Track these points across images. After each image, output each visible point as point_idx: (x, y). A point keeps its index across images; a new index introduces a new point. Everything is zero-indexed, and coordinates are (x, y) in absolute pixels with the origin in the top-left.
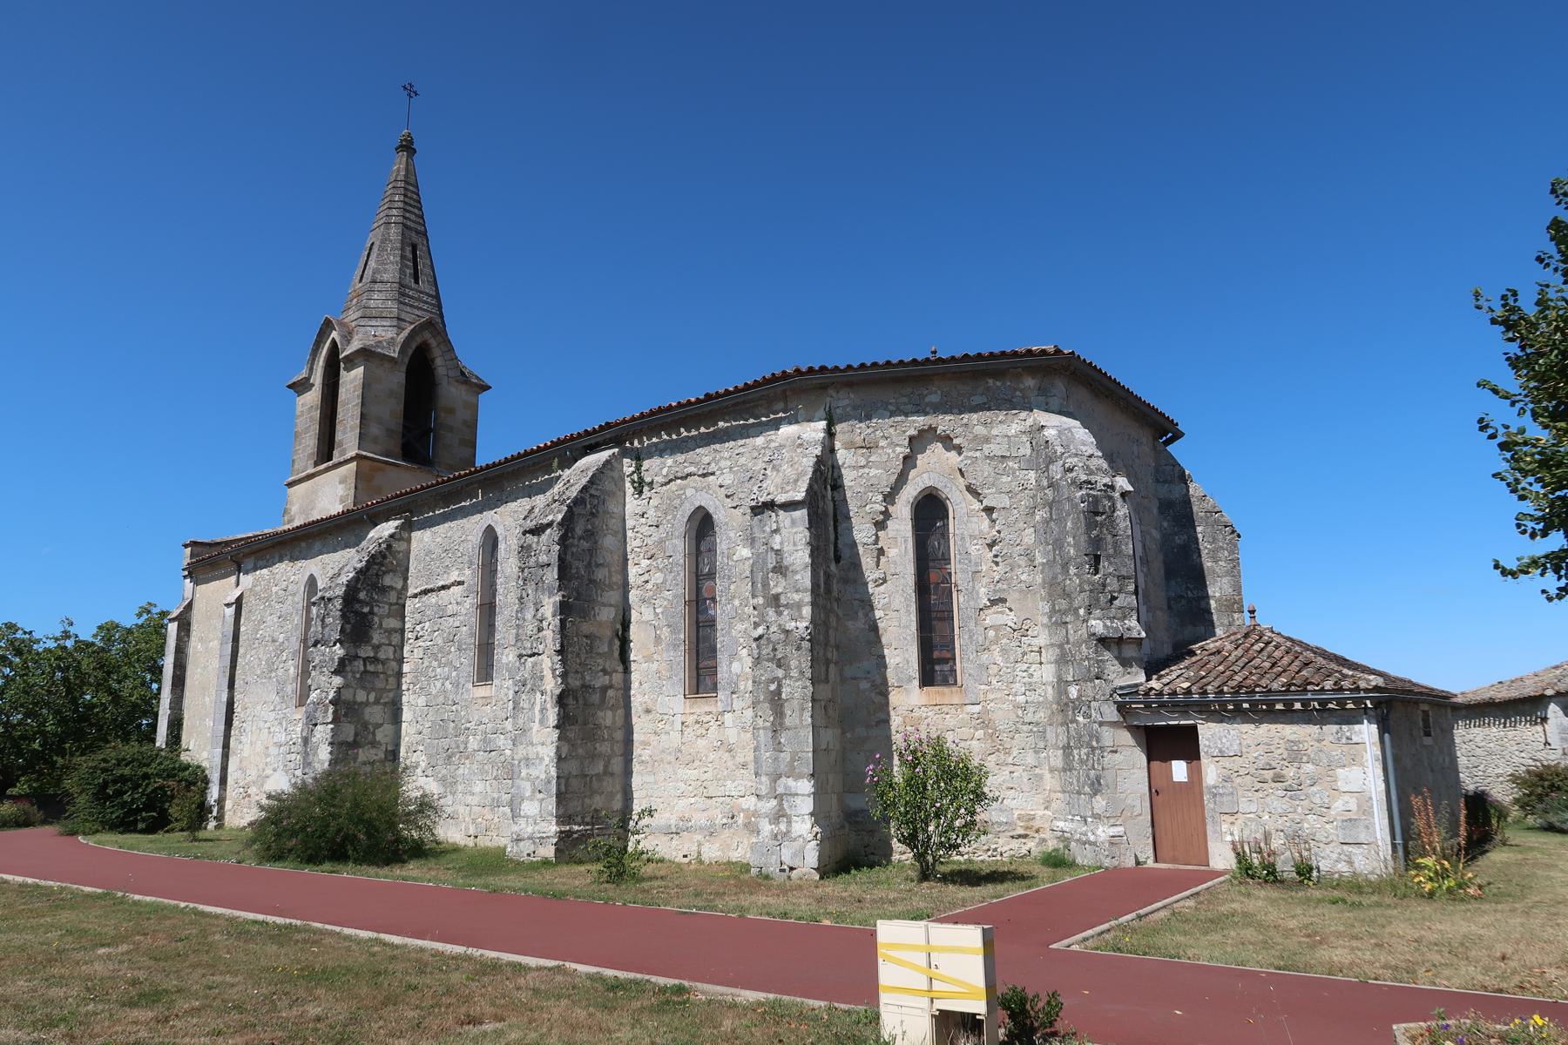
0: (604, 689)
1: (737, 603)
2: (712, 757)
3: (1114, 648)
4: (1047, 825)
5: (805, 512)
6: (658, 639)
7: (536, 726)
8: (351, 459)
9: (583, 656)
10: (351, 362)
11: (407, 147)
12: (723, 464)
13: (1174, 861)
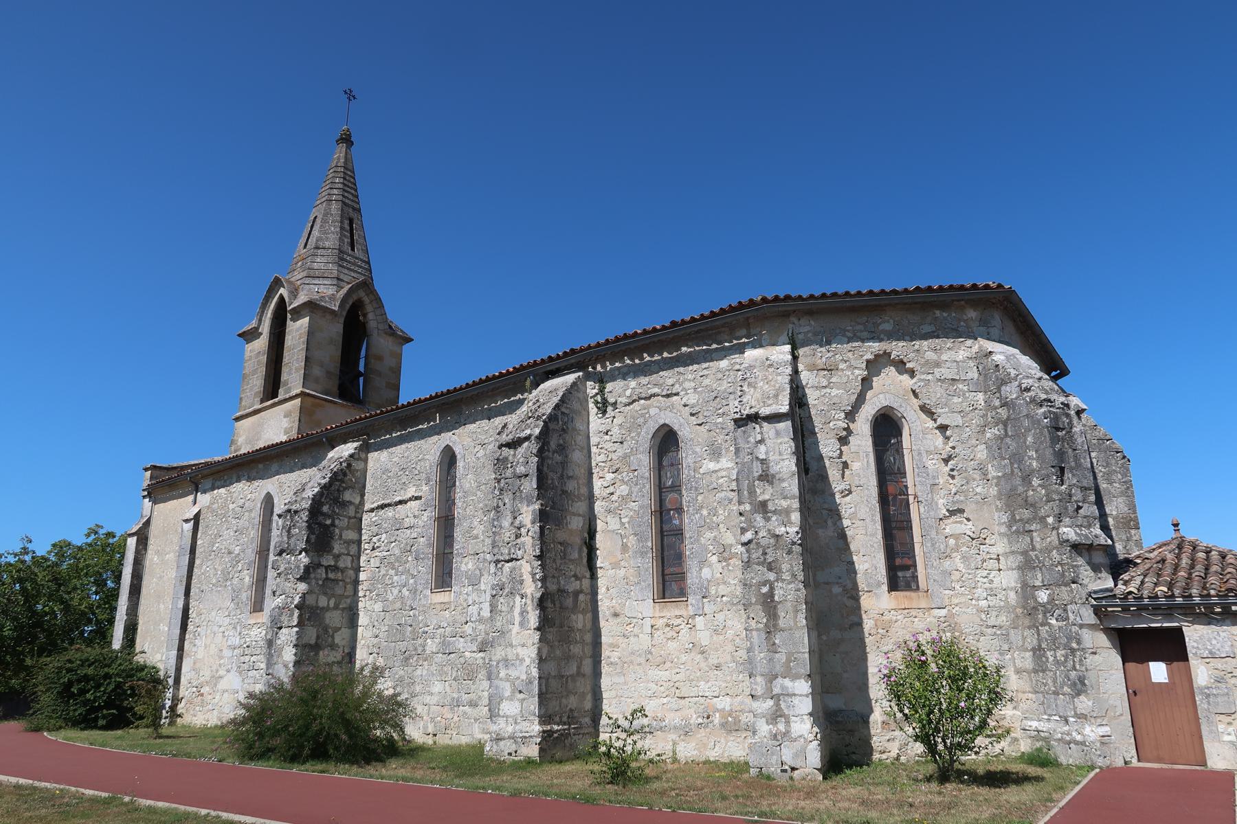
0: (577, 594)
1: (705, 512)
2: (684, 658)
3: (1086, 554)
4: (1017, 725)
5: (789, 423)
6: (625, 548)
7: (516, 628)
8: (296, 396)
9: (559, 562)
10: (297, 313)
11: (347, 140)
12: (687, 385)
13: (1159, 760)
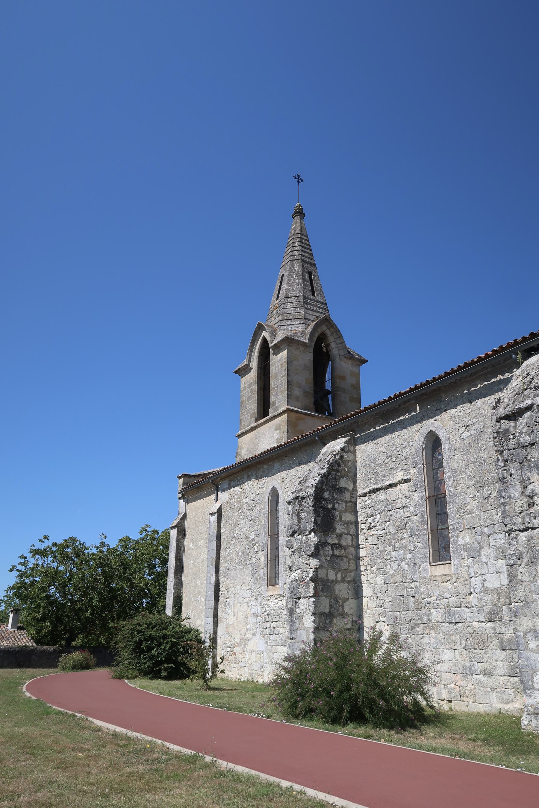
8: (283, 412)
10: (278, 348)
